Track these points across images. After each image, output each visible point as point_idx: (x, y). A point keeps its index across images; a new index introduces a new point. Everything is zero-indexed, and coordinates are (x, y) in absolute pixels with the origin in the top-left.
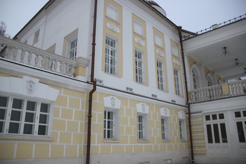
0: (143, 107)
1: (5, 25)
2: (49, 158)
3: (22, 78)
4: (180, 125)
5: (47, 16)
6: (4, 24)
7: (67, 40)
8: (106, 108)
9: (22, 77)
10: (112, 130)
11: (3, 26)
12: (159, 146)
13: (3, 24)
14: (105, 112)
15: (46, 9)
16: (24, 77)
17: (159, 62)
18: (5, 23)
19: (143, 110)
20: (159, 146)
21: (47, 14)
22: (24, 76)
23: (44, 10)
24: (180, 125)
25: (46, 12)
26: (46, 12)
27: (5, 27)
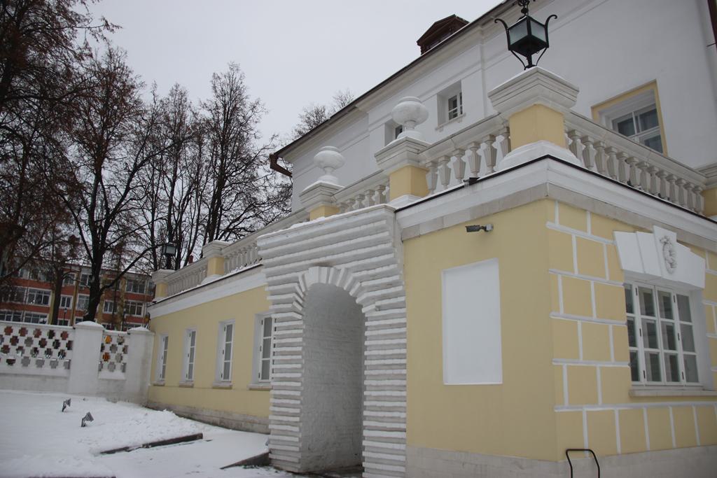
0: (668, 254)
1: (240, 72)
2: (618, 455)
3: (651, 232)
4: (227, 366)
5: (483, 44)
6: (237, 70)
7: (601, 113)
8: (629, 274)
9: (651, 229)
10: (694, 356)
11: (234, 76)
12: (599, 376)
13: (235, 69)
14: (628, 293)
15: (484, 24)
16: (656, 229)
17: (450, 110)
18: (241, 67)
19: (669, 266)
20: (599, 376)
21: (483, 38)
22: (655, 227)
23: (479, 28)
24: (227, 366)
25: (482, 33)
26: (482, 33)
27: (241, 77)
